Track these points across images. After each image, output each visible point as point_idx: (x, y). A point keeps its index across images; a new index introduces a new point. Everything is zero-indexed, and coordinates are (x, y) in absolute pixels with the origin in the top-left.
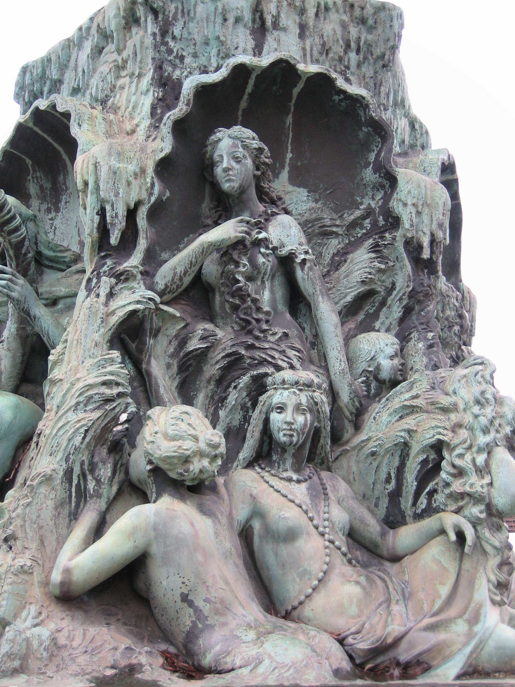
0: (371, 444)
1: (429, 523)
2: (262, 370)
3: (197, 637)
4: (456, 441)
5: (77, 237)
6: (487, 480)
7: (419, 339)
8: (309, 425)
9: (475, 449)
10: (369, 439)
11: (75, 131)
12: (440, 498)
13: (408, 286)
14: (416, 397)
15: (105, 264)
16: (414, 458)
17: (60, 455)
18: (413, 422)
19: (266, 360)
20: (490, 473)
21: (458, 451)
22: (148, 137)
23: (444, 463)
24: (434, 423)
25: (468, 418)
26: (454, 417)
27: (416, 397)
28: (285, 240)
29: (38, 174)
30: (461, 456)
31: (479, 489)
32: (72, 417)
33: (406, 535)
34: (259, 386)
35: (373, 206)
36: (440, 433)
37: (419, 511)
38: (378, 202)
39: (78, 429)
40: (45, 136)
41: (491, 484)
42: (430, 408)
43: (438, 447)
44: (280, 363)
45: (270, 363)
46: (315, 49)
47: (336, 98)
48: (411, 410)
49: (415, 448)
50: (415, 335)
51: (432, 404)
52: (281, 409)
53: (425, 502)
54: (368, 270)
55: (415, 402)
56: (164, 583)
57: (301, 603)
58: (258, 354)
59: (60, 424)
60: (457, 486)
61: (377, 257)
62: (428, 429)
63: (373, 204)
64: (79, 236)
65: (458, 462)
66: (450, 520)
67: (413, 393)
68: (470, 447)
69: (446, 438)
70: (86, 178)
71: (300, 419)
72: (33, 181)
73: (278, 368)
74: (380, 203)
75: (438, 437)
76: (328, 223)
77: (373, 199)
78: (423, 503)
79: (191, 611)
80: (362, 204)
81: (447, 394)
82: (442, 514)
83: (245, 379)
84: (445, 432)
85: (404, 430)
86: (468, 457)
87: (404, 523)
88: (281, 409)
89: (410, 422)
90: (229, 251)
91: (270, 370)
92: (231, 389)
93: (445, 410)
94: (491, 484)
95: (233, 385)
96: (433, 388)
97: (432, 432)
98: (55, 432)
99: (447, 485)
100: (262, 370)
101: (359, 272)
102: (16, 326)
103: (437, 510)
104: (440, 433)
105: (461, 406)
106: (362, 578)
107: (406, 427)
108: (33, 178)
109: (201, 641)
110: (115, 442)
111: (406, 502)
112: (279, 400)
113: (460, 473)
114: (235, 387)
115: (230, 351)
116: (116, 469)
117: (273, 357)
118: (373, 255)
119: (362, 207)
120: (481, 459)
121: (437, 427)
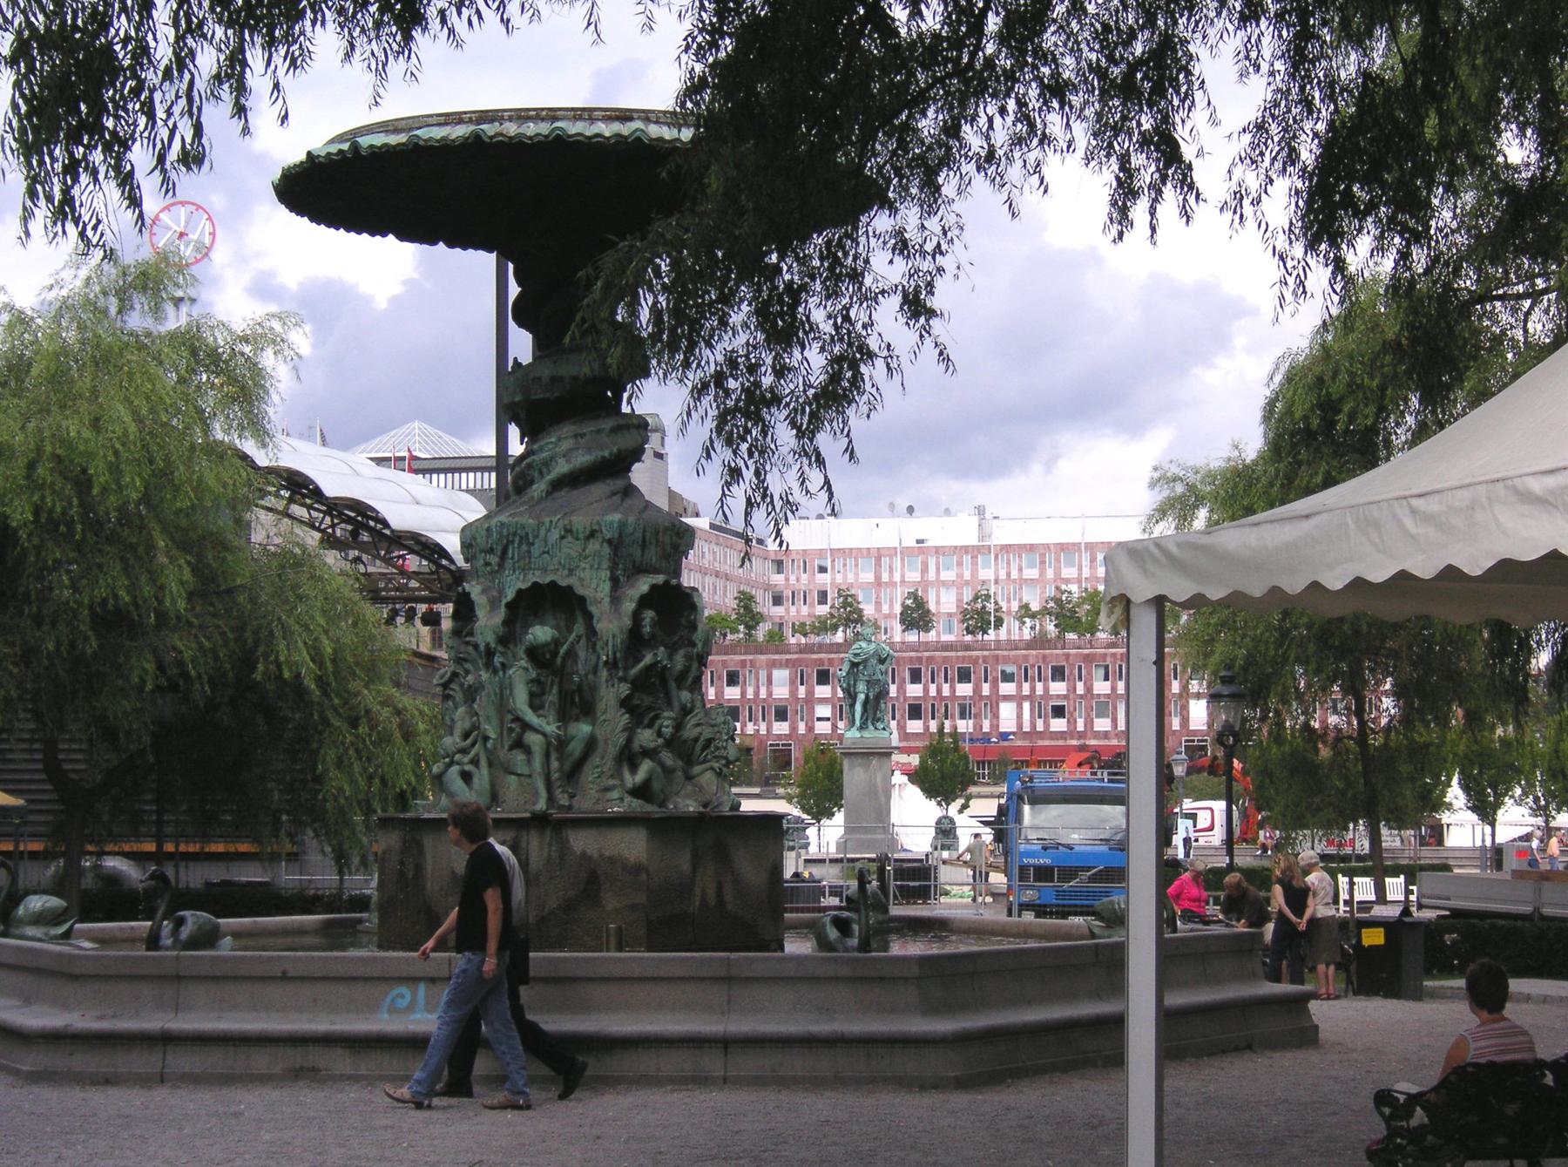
33: (697, 769)
34: (657, 717)
43: (709, 742)
62: (707, 733)
89: (698, 729)
116: (629, 757)
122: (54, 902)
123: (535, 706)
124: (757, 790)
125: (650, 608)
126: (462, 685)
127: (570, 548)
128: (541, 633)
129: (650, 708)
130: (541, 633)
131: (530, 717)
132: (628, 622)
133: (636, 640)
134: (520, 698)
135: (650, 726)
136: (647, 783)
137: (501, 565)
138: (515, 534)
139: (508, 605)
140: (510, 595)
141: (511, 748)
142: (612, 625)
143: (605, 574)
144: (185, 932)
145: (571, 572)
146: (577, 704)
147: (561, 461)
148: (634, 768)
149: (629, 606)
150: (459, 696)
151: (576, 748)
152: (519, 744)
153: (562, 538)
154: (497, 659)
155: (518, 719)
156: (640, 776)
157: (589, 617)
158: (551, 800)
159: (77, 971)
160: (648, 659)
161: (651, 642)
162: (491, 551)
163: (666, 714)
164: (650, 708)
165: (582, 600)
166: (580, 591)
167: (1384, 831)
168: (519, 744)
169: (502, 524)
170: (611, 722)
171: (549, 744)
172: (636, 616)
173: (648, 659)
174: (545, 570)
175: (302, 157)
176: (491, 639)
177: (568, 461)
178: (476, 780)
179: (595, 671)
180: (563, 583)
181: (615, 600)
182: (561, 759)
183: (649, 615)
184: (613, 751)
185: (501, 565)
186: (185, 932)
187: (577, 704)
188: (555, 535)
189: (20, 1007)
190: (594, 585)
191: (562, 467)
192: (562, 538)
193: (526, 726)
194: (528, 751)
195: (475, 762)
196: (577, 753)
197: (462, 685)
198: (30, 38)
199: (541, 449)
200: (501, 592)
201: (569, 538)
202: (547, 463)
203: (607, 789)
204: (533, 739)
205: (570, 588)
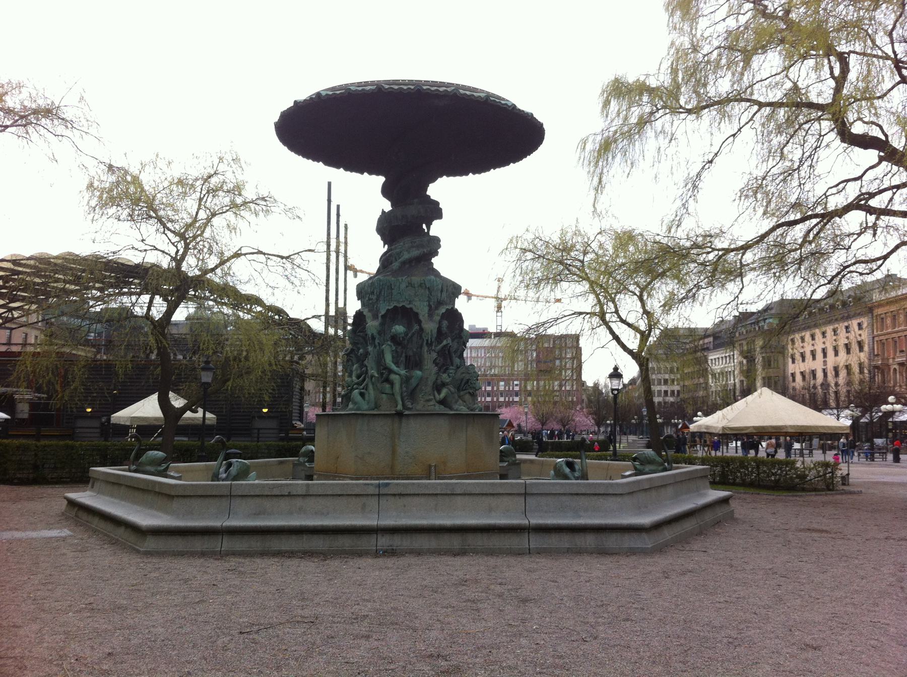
34: (447, 369)
43: (468, 380)
90: (445, 346)
122: (160, 454)
123: (397, 364)
126: (356, 355)
128: (399, 329)
130: (399, 329)
131: (394, 367)
134: (388, 358)
135: (444, 372)
136: (445, 398)
137: (377, 299)
139: (382, 316)
140: (383, 312)
141: (383, 382)
142: (430, 327)
143: (426, 304)
144: (233, 470)
145: (410, 302)
146: (413, 363)
147: (405, 253)
148: (439, 393)
149: (438, 318)
150: (354, 360)
151: (414, 382)
152: (387, 380)
154: (377, 341)
155: (386, 368)
156: (442, 395)
157: (419, 322)
158: (403, 405)
159: (173, 493)
160: (445, 342)
162: (372, 293)
165: (417, 314)
166: (415, 310)
167: (171, 395)
168: (387, 380)
169: (380, 280)
170: (430, 368)
171: (402, 379)
173: (445, 342)
174: (398, 302)
175: (292, 104)
176: (375, 332)
177: (409, 253)
178: (366, 396)
179: (421, 347)
180: (408, 306)
181: (431, 315)
182: (407, 388)
183: (445, 323)
184: (430, 383)
185: (377, 299)
186: (233, 470)
187: (413, 363)
188: (403, 286)
191: (406, 256)
193: (391, 371)
194: (392, 384)
195: (366, 388)
196: (414, 385)
197: (356, 355)
199: (396, 248)
200: (378, 311)
202: (399, 254)
203: (429, 400)
204: (393, 377)
205: (411, 309)
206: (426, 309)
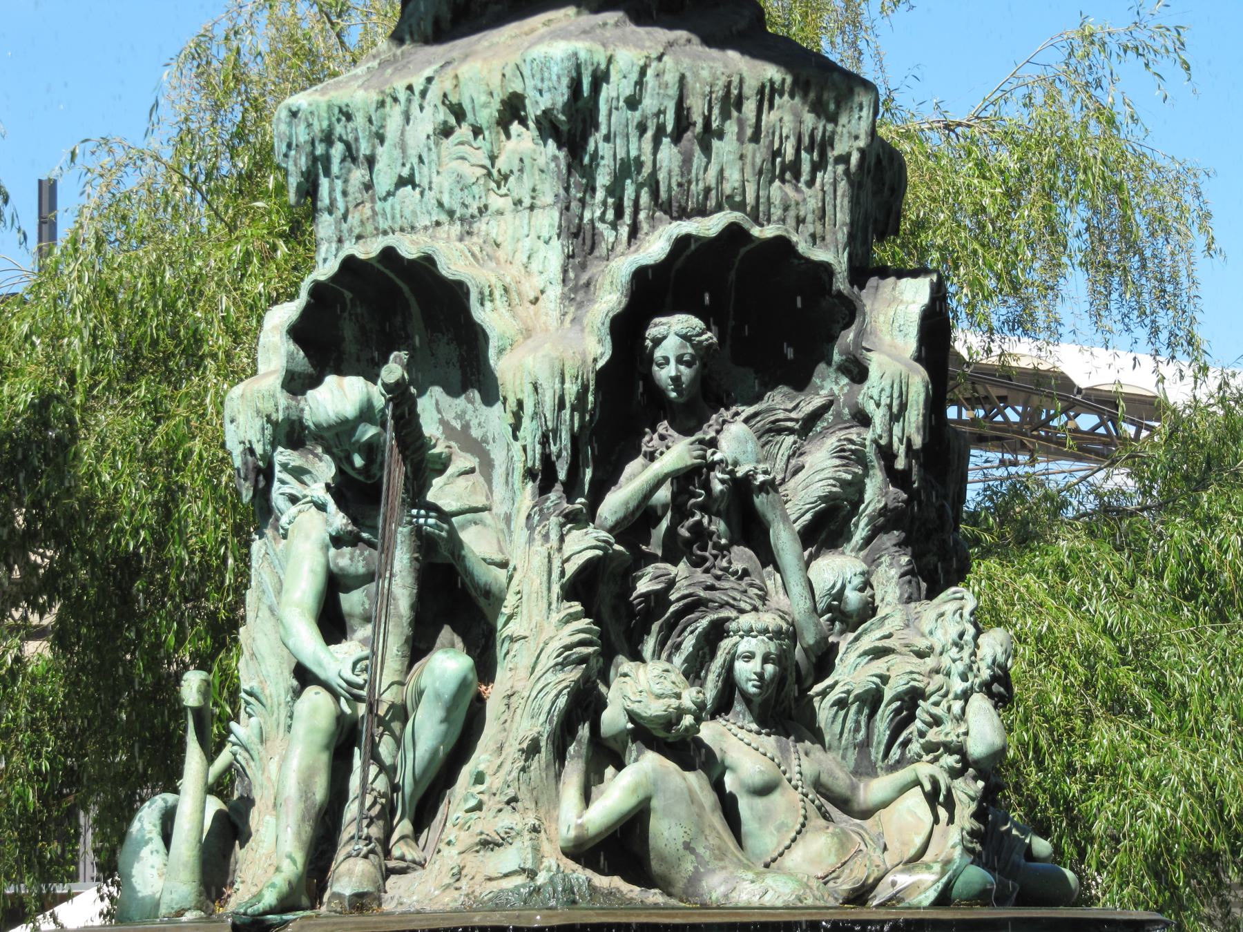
0: (838, 689)
1: (905, 774)
2: (724, 613)
3: (700, 881)
4: (929, 689)
5: (435, 412)
6: (962, 730)
7: (891, 564)
8: (655, 627)
9: (951, 696)
10: (836, 683)
11: (482, 315)
12: (915, 747)
13: (879, 501)
14: (889, 636)
15: (548, 498)
16: (887, 705)
17: (543, 718)
18: (884, 666)
19: (728, 603)
20: (966, 721)
21: (934, 698)
22: (564, 314)
23: (918, 712)
24: (909, 668)
25: (946, 661)
26: (930, 662)
27: (889, 636)
28: (741, 458)
29: (359, 310)
30: (937, 704)
31: (955, 738)
32: (550, 677)
33: (874, 789)
34: (718, 631)
35: (837, 392)
36: (915, 680)
37: (892, 762)
38: (842, 389)
39: (561, 692)
40: (387, 272)
41: (966, 734)
42: (905, 650)
44: (743, 605)
45: (732, 606)
46: (758, 155)
47: (796, 261)
48: (878, 653)
49: (888, 693)
50: (886, 559)
51: (907, 646)
52: (750, 657)
53: (899, 752)
54: (832, 482)
55: (886, 643)
56: (666, 834)
57: (781, 855)
58: (717, 595)
59: (539, 686)
60: (933, 735)
61: (843, 465)
63: (836, 389)
64: (439, 411)
65: (934, 710)
66: (924, 770)
67: (885, 631)
68: (946, 695)
69: (921, 685)
70: (520, 396)
71: (770, 668)
72: (351, 320)
73: (742, 611)
74: (846, 390)
75: (913, 683)
76: (781, 416)
77: (837, 383)
78: (895, 753)
79: (693, 857)
80: (822, 388)
81: (923, 635)
82: (917, 765)
83: (704, 623)
84: (921, 678)
85: (876, 676)
86: (944, 704)
87: (876, 775)
88: (750, 657)
89: (880, 666)
91: (733, 614)
92: (686, 634)
93: (921, 655)
94: (966, 734)
95: (689, 629)
96: (907, 626)
97: (907, 678)
98: (534, 694)
99: (922, 734)
100: (724, 613)
101: (821, 484)
102: (408, 556)
103: (912, 761)
104: (915, 680)
105: (938, 649)
106: (989, 671)
107: (878, 672)
108: (350, 315)
109: (704, 884)
110: (584, 703)
111: (876, 753)
112: (747, 649)
113: (937, 721)
114: (692, 632)
115: (686, 592)
117: (734, 599)
118: (838, 462)
119: (822, 392)
120: (957, 706)
121: (912, 673)
124: (576, 425)
125: (903, 471)
127: (458, 163)
129: (694, 605)
132: (597, 348)
133: (620, 406)
138: (328, 139)
139: (318, 290)
143: (547, 220)
149: (609, 299)
153: (446, 132)
161: (691, 411)
163: (746, 620)
164: (694, 605)
172: (627, 331)
189: (206, 783)
190: (522, 257)
192: (446, 132)
198: (20, 463)
201: (464, 131)
206: (553, 256)
